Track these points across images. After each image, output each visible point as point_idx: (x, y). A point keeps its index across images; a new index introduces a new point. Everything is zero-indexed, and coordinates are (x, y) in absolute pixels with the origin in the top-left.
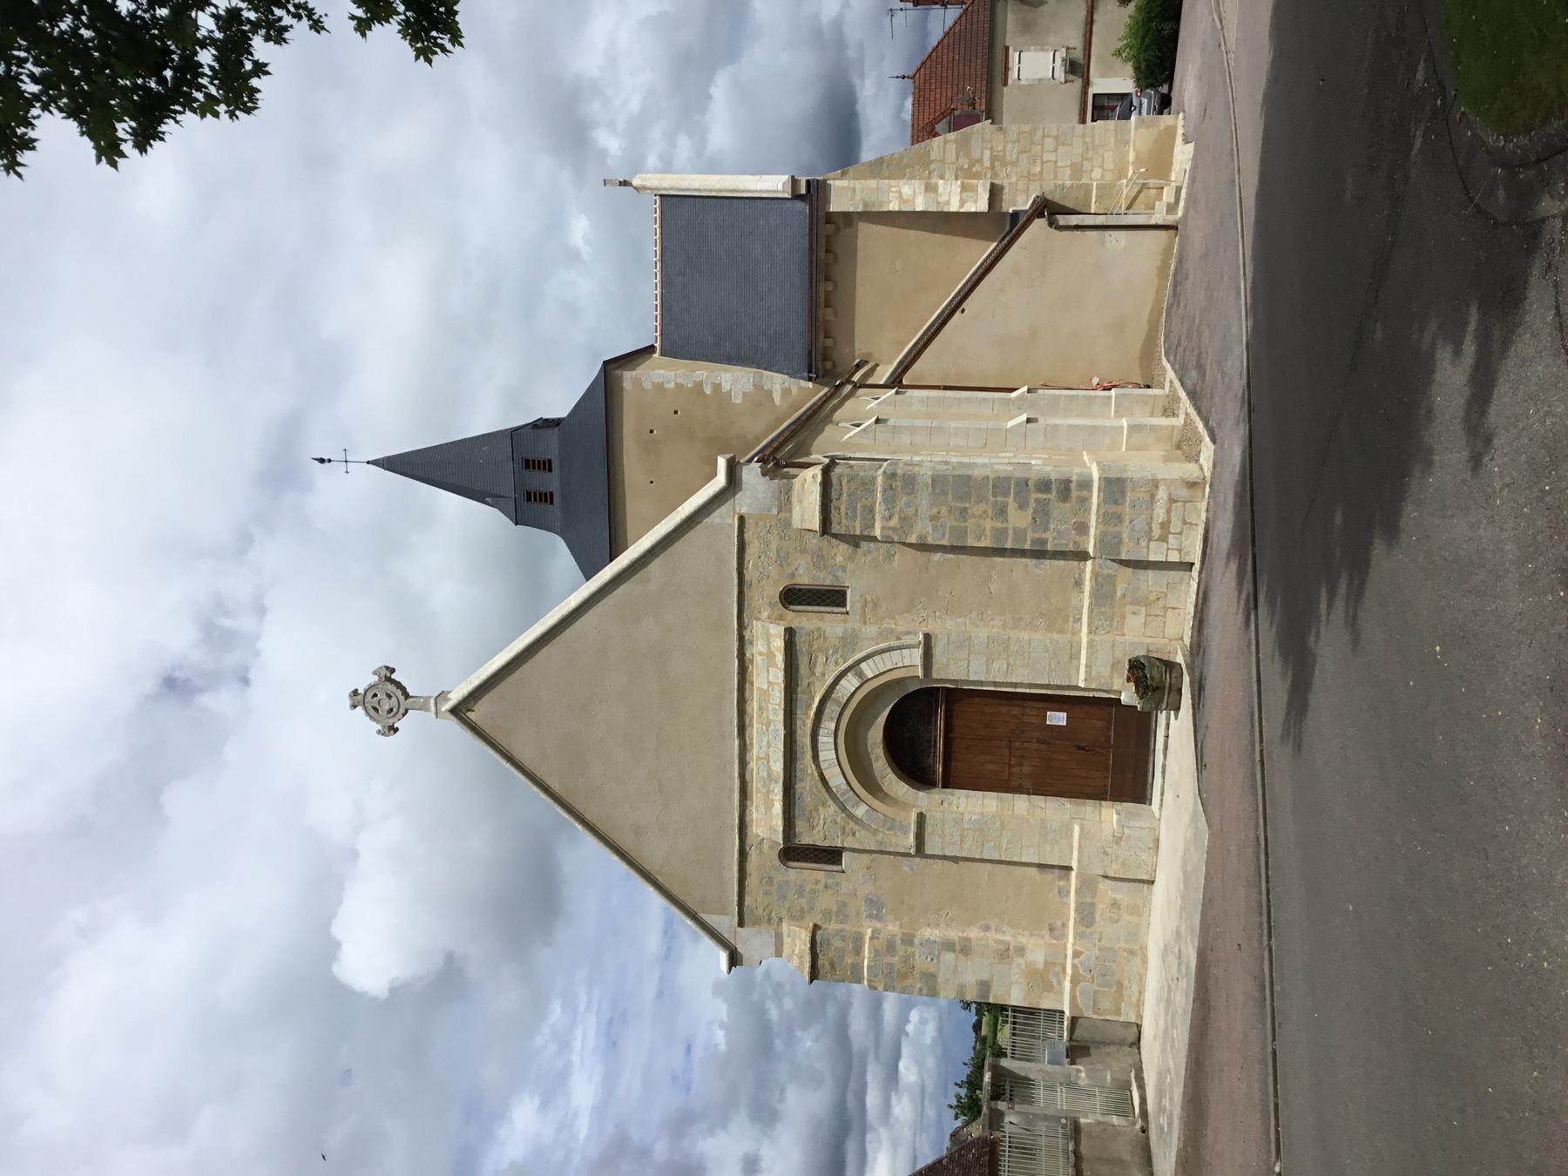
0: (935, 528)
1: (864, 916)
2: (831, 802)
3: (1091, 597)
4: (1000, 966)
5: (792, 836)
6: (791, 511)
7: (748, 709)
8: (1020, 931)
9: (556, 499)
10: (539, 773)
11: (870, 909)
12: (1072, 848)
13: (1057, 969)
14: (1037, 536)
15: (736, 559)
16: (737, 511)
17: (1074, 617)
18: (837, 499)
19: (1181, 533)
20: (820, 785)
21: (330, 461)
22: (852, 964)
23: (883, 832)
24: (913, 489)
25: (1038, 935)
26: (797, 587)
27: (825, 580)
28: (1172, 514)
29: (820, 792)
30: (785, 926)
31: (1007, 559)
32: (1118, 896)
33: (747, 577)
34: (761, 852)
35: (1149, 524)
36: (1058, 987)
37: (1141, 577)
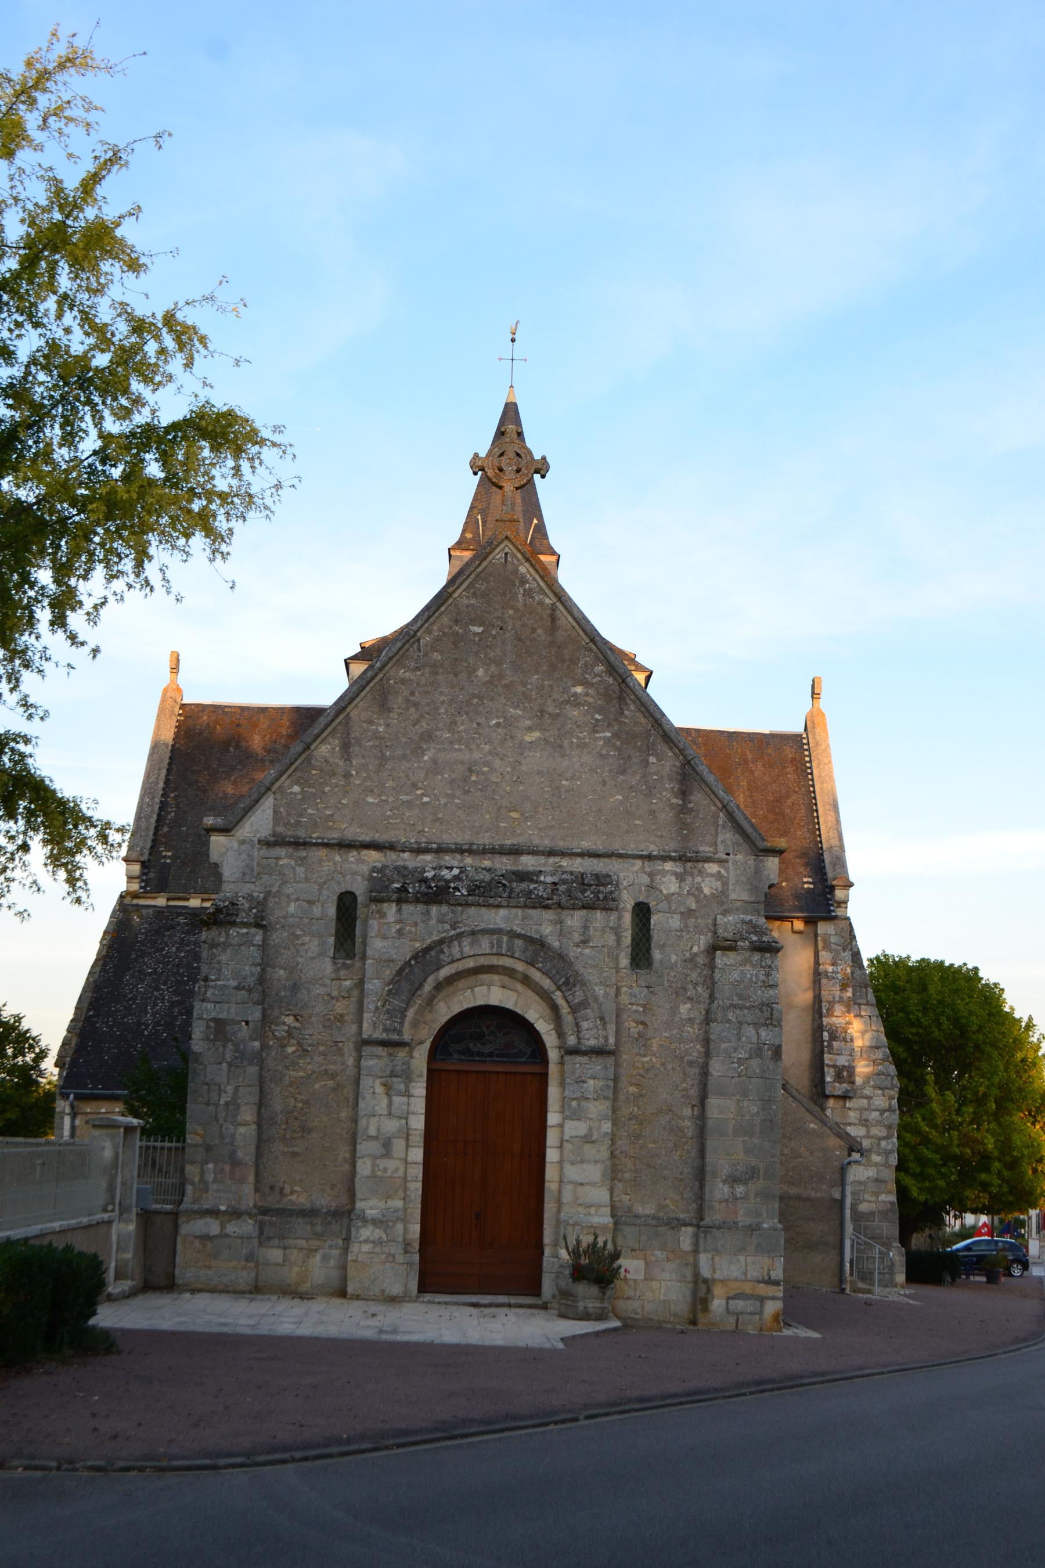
21: (513, 340)
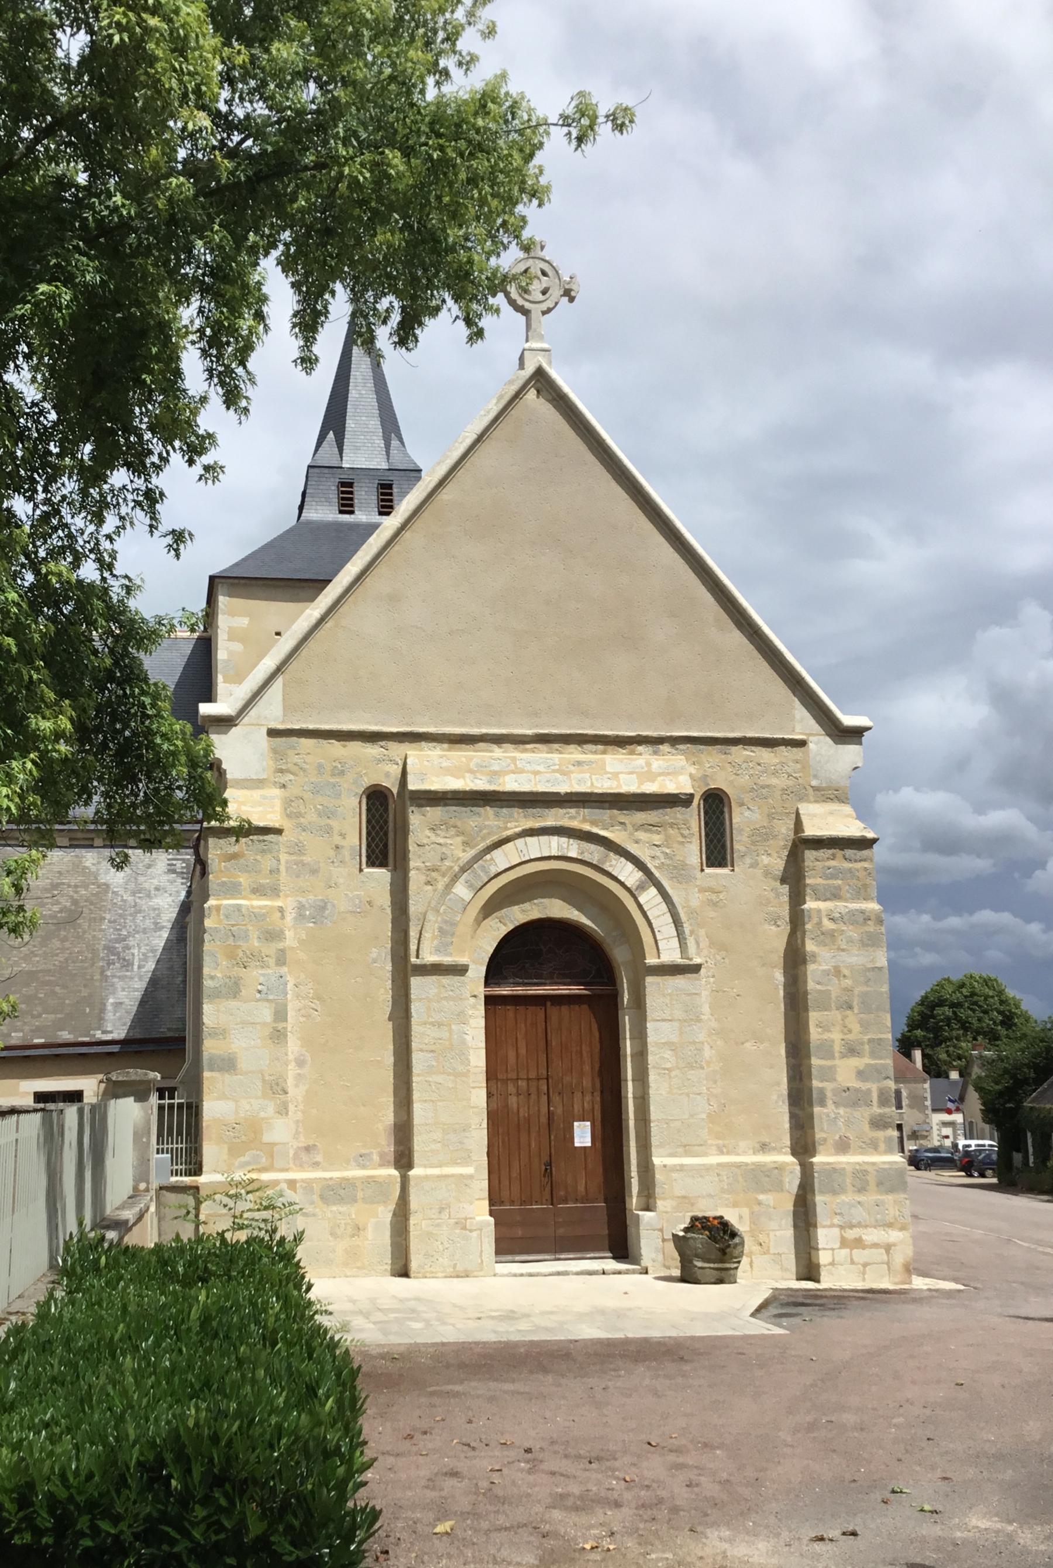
0: (827, 973)
1: (301, 899)
2: (472, 853)
3: (753, 1164)
4: (259, 1084)
5: (420, 801)
6: (816, 801)
7: (572, 747)
8: (301, 1107)
9: (346, 518)
10: (461, 473)
11: (311, 906)
12: (440, 1165)
13: (264, 1160)
14: (829, 1094)
15: (757, 735)
16: (811, 738)
17: (724, 1146)
18: (844, 856)
19: (852, 1262)
20: (495, 838)
22: (240, 884)
23: (436, 922)
24: (868, 945)
25: (297, 1133)
26: (726, 810)
27: (740, 842)
28: (873, 1250)
29: (483, 839)
30: (277, 792)
31: (785, 1061)
32: (370, 1233)
33: (734, 749)
34: (379, 761)
35: (859, 1225)
36: (237, 1163)
37: (783, 1222)
